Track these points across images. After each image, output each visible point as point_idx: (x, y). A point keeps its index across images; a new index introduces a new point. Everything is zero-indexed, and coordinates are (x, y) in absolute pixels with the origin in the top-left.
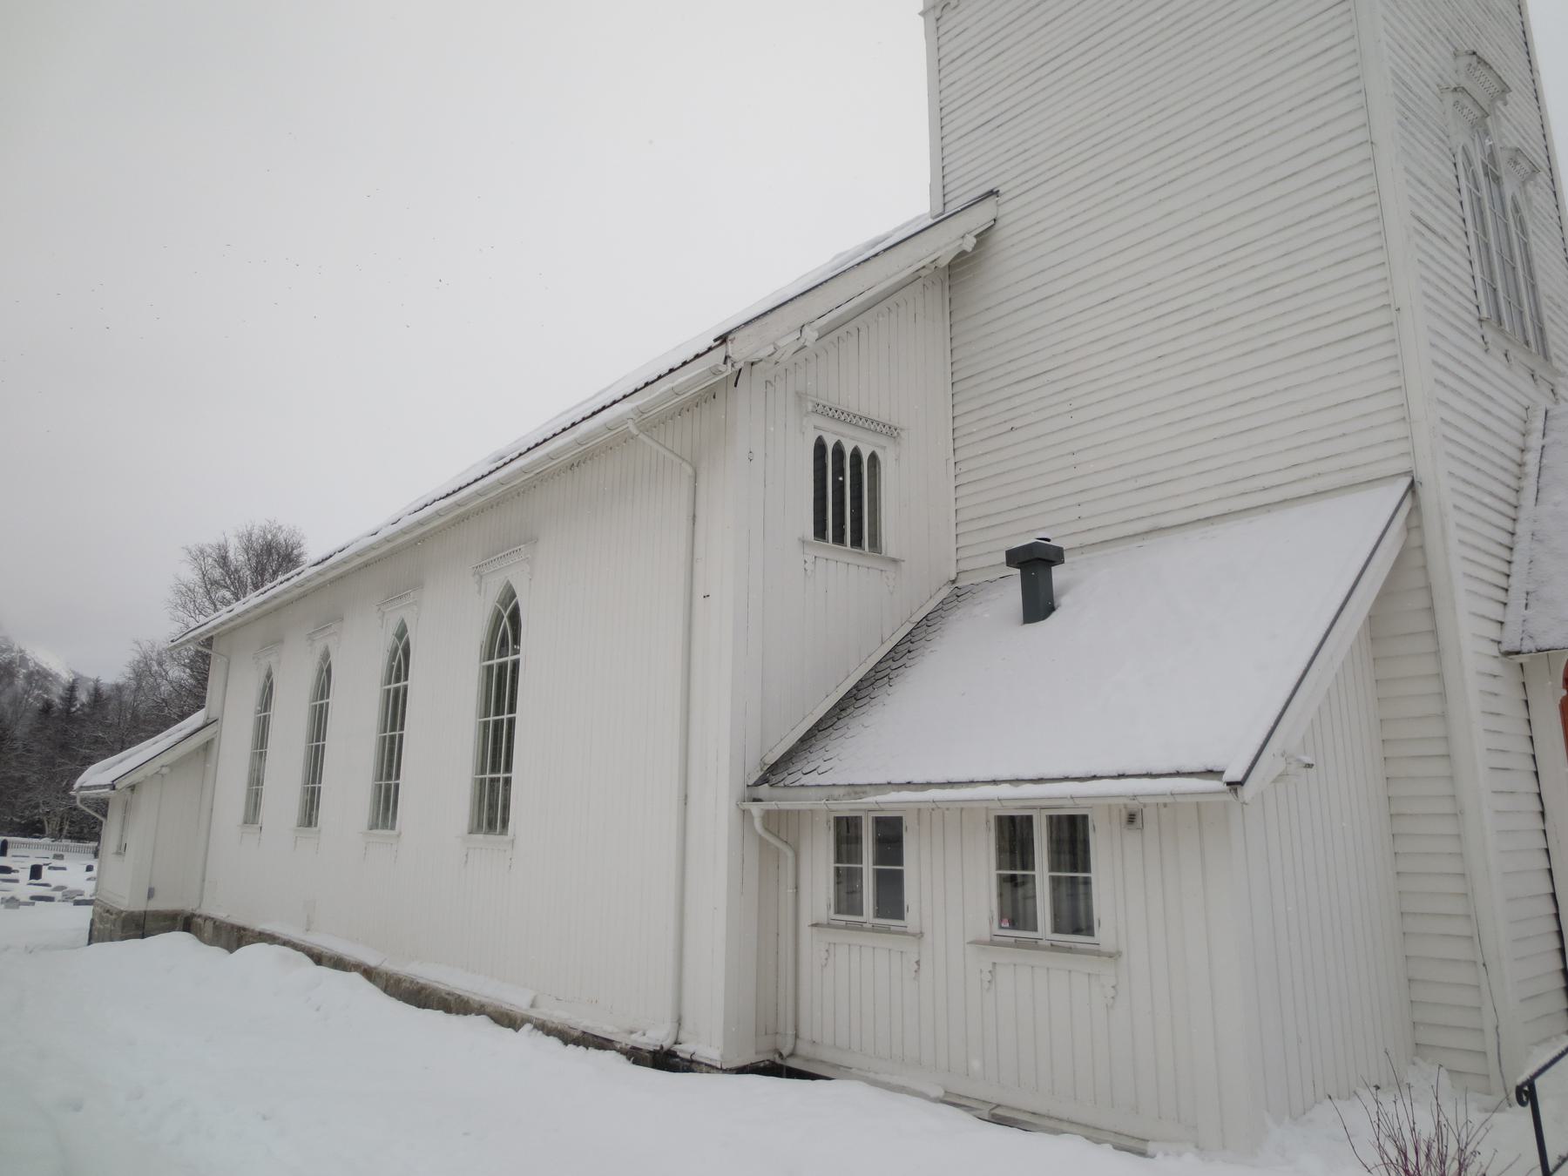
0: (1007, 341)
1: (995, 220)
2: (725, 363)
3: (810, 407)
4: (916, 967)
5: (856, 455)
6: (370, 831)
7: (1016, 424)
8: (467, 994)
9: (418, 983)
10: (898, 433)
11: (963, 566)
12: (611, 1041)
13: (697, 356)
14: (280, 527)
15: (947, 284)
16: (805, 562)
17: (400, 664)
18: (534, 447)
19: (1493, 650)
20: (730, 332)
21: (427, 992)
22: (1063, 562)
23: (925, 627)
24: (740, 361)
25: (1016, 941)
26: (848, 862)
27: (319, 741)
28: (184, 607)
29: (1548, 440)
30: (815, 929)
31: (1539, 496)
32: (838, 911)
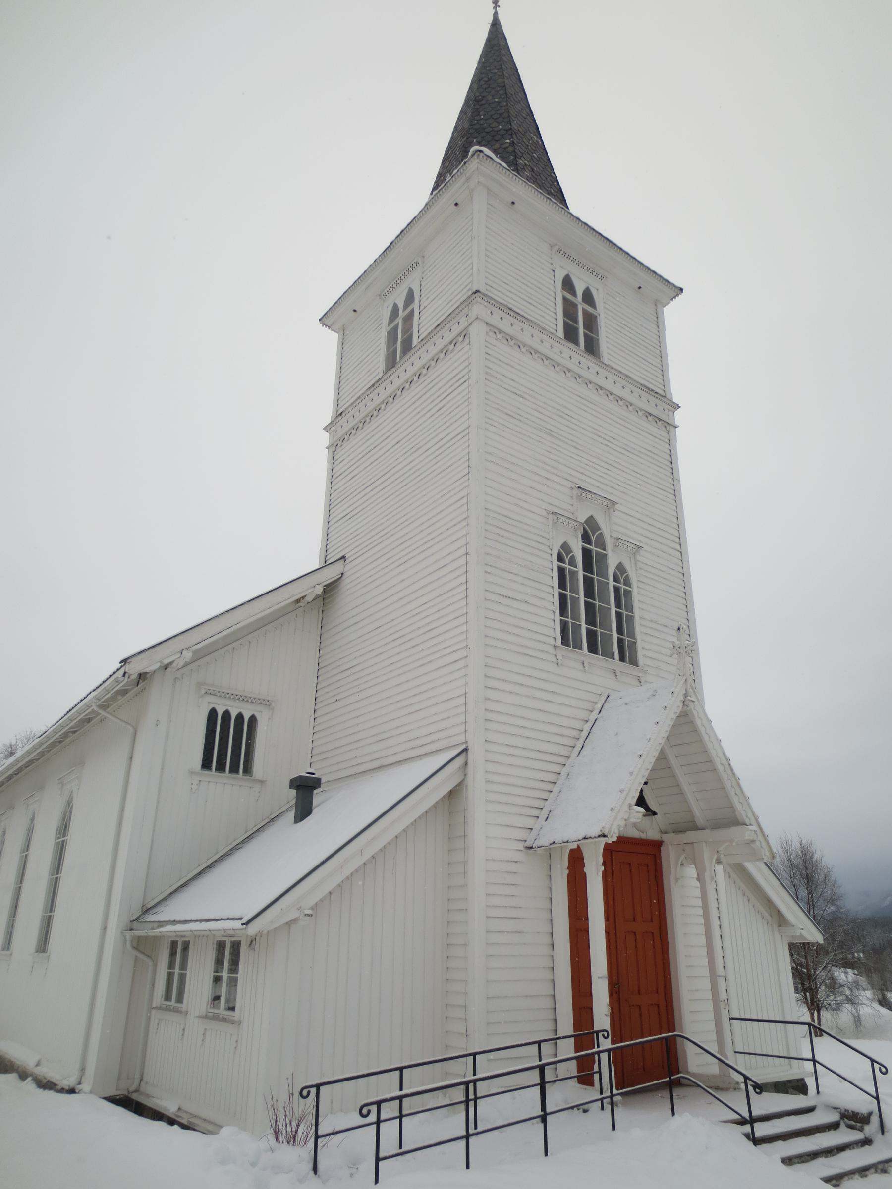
0: (340, 647)
1: (342, 574)
3: (203, 691)
5: (240, 717)
7: (338, 697)
10: (270, 703)
12: (56, 1085)
16: (192, 784)
17: (64, 829)
19: (521, 846)
25: (213, 1015)
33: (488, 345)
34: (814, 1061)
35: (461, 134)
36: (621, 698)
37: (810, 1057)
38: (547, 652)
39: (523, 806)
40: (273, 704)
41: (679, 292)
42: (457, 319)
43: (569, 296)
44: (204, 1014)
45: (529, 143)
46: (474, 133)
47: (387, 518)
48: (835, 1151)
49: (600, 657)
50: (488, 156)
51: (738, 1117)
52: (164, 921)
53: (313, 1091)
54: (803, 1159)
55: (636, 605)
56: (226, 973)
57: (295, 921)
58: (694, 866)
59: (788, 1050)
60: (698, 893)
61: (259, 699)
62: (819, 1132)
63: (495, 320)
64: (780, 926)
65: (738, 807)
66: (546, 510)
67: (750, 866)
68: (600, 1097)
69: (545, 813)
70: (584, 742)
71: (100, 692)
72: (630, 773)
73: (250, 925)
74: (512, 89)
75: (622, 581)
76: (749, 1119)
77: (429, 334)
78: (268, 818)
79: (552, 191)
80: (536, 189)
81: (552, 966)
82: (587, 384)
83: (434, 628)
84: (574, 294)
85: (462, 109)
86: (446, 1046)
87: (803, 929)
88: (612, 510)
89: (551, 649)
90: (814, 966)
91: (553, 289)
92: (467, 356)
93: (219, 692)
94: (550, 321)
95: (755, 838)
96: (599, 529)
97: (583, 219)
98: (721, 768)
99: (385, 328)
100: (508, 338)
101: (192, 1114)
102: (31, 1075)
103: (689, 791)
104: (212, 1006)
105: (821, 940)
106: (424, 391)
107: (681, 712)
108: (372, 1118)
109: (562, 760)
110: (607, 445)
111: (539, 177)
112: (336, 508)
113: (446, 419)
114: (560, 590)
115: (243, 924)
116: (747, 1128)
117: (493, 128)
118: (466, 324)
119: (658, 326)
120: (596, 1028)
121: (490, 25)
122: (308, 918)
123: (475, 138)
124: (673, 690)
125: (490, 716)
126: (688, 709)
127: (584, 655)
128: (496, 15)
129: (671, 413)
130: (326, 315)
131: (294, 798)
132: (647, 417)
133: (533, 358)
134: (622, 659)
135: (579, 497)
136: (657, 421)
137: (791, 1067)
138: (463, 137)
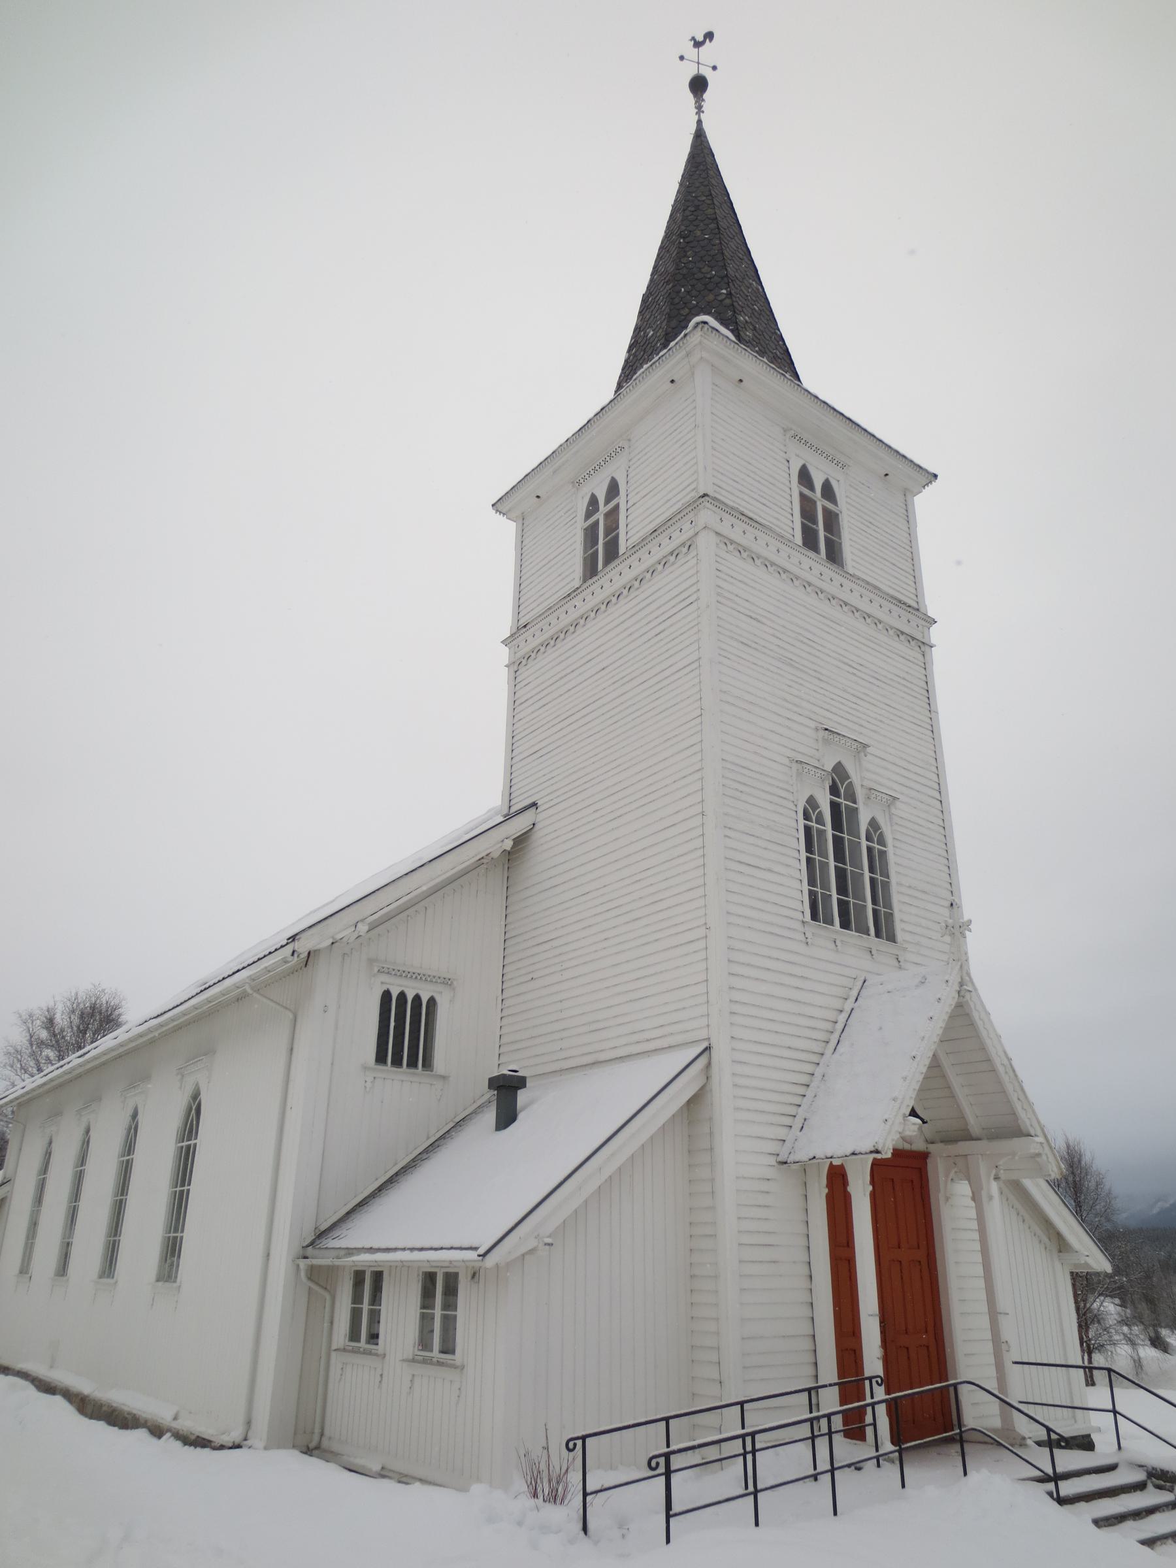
3: (376, 970)
5: (417, 998)
8: (139, 1413)
9: (112, 1406)
12: (210, 1441)
14: (103, 990)
16: (366, 1081)
17: (190, 1126)
18: (279, 949)
19: (772, 1161)
20: (296, 935)
21: (117, 1413)
22: (525, 1087)
24: (304, 952)
27: (123, 1196)
28: (12, 1067)
31: (837, 1048)
33: (719, 560)
34: (1115, 1412)
35: (665, 278)
36: (881, 984)
38: (794, 930)
39: (774, 1113)
40: (455, 983)
41: (933, 479)
42: (678, 525)
43: (807, 492)
44: (411, 1357)
45: (748, 292)
46: (681, 279)
47: (593, 760)
48: (1144, 1513)
49: (854, 933)
50: (713, 328)
51: (1040, 1474)
52: (355, 1249)
53: (579, 1443)
54: (1110, 1521)
55: (893, 869)
56: (440, 1310)
57: (532, 1251)
58: (967, 1182)
59: (1072, 1398)
60: (973, 1214)
61: (439, 978)
62: (1124, 1493)
63: (725, 529)
64: (1060, 1251)
65: (1022, 1114)
66: (788, 757)
67: (1028, 1183)
68: (874, 1454)
69: (798, 1123)
70: (840, 1037)
71: (259, 971)
72: (903, 1078)
73: (488, 1257)
74: (725, 221)
75: (876, 839)
76: (1052, 1475)
78: (452, 1121)
79: (778, 353)
80: (768, 365)
81: (811, 1301)
82: (829, 600)
83: (661, 900)
84: (812, 488)
85: (662, 243)
86: (693, 1394)
87: (1088, 1256)
89: (798, 926)
90: (1084, 1297)
91: (788, 483)
92: (693, 571)
93: (394, 970)
94: (787, 525)
95: (1041, 1152)
96: (848, 777)
98: (1001, 1069)
99: (580, 524)
100: (741, 549)
101: (400, 1474)
102: (169, 1430)
103: (961, 1093)
104: (420, 1348)
105: (1108, 1268)
106: (637, 608)
107: (957, 1003)
108: (662, 1469)
109: (815, 1058)
110: (854, 674)
111: (762, 336)
112: (520, 742)
113: (670, 645)
114: (807, 854)
115: (479, 1256)
116: (1051, 1486)
118: (691, 533)
119: (908, 522)
120: (867, 1374)
121: (692, 136)
122: (547, 1247)
123: (683, 286)
124: (946, 978)
125: (737, 1008)
126: (965, 1000)
128: (699, 122)
129: (926, 629)
130: (501, 501)
131: (523, 1109)
132: (898, 636)
133: (770, 572)
134: (878, 935)
135: (826, 741)
136: (911, 640)
137: (1076, 1422)
138: (668, 283)
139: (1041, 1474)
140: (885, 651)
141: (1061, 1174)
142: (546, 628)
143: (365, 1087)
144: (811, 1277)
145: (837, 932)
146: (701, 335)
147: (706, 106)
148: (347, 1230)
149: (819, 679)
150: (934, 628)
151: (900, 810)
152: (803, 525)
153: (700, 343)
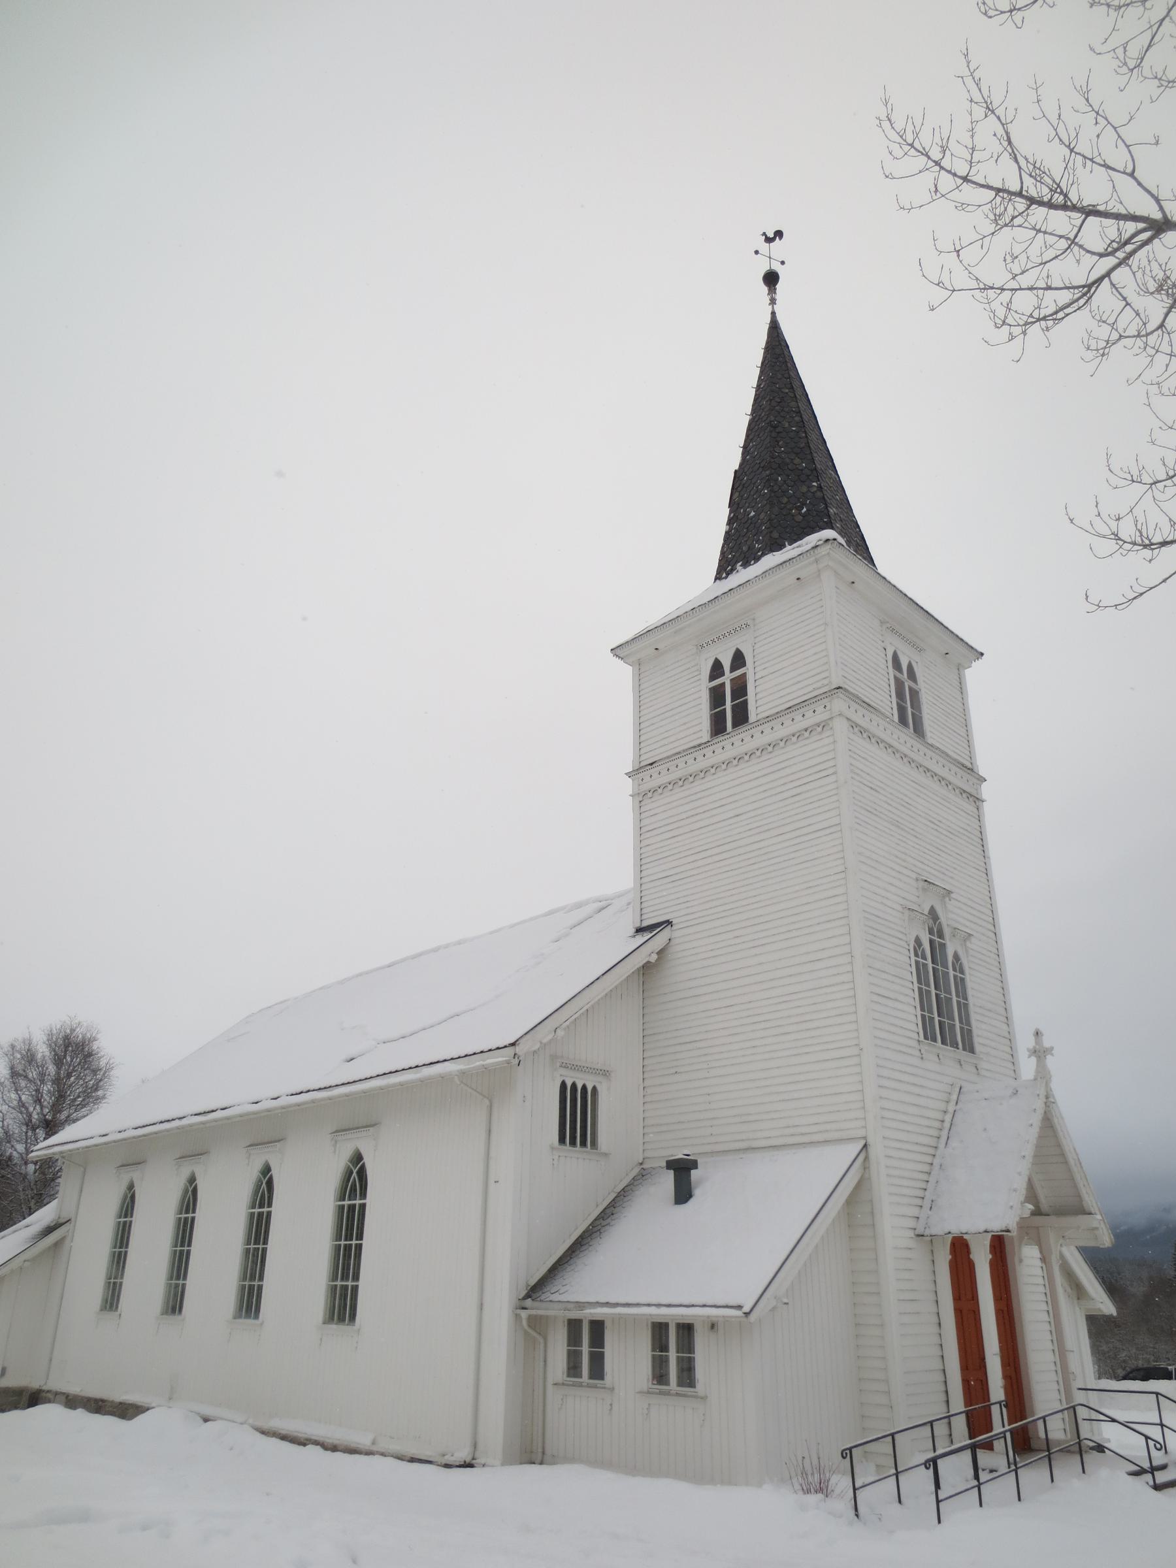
2: (514, 1058)
3: (558, 1064)
4: (610, 1407)
5: (584, 1088)
6: (235, 1320)
9: (280, 1434)
11: (647, 1154)
13: (498, 1048)
15: (642, 972)
16: (553, 1160)
19: (911, 1234)
23: (622, 1197)
26: (575, 1346)
29: (958, 1107)
30: (555, 1386)
32: (569, 1375)
34: (1162, 1425)
37: (1159, 1422)
42: (813, 706)
43: (898, 675)
49: (949, 1048)
50: (840, 544)
51: (1137, 1468)
53: (848, 1452)
63: (850, 714)
69: (927, 1203)
75: (920, 954)
77: (777, 713)
78: (613, 1191)
88: (947, 899)
89: (915, 1044)
97: (909, 595)
98: (1072, 1162)
116: (1149, 1477)
117: (796, 465)
120: (993, 1400)
127: (939, 1048)
128: (773, 313)
135: (924, 890)
139: (1139, 1468)
140: (953, 808)
141: (1112, 1243)
142: (673, 768)
143: (553, 1164)
144: (940, 1324)
145: (939, 1048)
146: (830, 549)
147: (777, 297)
148: (563, 1286)
149: (915, 836)
150: (984, 784)
151: (973, 944)
152: (898, 704)
153: (828, 554)
